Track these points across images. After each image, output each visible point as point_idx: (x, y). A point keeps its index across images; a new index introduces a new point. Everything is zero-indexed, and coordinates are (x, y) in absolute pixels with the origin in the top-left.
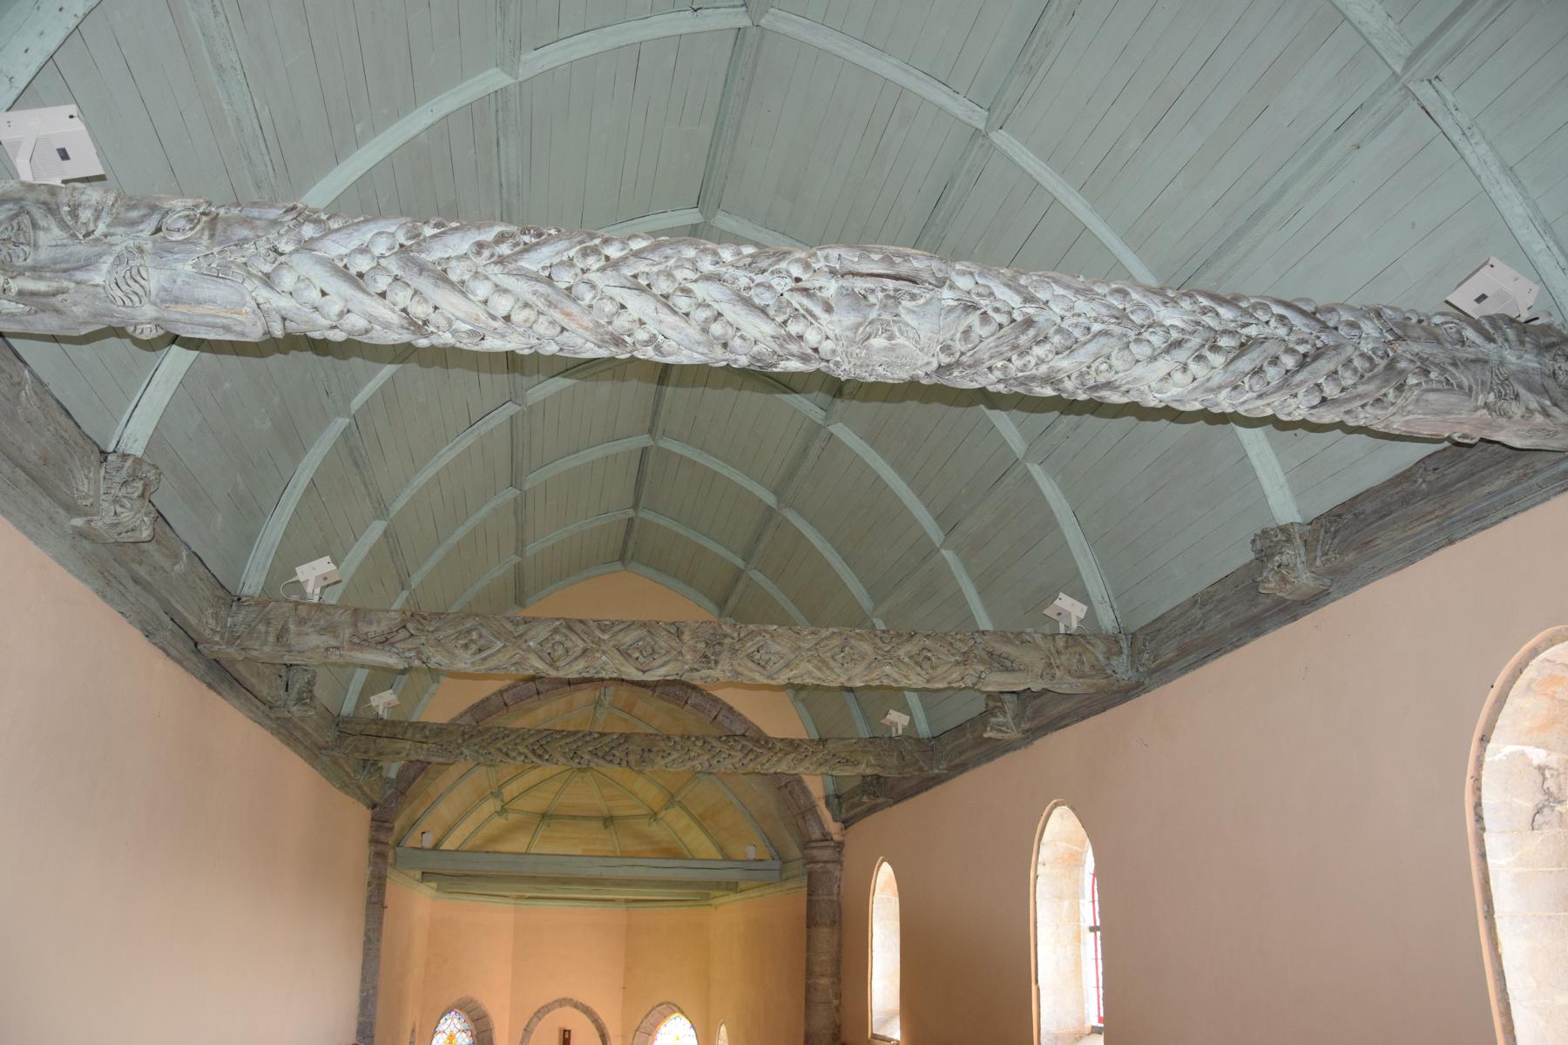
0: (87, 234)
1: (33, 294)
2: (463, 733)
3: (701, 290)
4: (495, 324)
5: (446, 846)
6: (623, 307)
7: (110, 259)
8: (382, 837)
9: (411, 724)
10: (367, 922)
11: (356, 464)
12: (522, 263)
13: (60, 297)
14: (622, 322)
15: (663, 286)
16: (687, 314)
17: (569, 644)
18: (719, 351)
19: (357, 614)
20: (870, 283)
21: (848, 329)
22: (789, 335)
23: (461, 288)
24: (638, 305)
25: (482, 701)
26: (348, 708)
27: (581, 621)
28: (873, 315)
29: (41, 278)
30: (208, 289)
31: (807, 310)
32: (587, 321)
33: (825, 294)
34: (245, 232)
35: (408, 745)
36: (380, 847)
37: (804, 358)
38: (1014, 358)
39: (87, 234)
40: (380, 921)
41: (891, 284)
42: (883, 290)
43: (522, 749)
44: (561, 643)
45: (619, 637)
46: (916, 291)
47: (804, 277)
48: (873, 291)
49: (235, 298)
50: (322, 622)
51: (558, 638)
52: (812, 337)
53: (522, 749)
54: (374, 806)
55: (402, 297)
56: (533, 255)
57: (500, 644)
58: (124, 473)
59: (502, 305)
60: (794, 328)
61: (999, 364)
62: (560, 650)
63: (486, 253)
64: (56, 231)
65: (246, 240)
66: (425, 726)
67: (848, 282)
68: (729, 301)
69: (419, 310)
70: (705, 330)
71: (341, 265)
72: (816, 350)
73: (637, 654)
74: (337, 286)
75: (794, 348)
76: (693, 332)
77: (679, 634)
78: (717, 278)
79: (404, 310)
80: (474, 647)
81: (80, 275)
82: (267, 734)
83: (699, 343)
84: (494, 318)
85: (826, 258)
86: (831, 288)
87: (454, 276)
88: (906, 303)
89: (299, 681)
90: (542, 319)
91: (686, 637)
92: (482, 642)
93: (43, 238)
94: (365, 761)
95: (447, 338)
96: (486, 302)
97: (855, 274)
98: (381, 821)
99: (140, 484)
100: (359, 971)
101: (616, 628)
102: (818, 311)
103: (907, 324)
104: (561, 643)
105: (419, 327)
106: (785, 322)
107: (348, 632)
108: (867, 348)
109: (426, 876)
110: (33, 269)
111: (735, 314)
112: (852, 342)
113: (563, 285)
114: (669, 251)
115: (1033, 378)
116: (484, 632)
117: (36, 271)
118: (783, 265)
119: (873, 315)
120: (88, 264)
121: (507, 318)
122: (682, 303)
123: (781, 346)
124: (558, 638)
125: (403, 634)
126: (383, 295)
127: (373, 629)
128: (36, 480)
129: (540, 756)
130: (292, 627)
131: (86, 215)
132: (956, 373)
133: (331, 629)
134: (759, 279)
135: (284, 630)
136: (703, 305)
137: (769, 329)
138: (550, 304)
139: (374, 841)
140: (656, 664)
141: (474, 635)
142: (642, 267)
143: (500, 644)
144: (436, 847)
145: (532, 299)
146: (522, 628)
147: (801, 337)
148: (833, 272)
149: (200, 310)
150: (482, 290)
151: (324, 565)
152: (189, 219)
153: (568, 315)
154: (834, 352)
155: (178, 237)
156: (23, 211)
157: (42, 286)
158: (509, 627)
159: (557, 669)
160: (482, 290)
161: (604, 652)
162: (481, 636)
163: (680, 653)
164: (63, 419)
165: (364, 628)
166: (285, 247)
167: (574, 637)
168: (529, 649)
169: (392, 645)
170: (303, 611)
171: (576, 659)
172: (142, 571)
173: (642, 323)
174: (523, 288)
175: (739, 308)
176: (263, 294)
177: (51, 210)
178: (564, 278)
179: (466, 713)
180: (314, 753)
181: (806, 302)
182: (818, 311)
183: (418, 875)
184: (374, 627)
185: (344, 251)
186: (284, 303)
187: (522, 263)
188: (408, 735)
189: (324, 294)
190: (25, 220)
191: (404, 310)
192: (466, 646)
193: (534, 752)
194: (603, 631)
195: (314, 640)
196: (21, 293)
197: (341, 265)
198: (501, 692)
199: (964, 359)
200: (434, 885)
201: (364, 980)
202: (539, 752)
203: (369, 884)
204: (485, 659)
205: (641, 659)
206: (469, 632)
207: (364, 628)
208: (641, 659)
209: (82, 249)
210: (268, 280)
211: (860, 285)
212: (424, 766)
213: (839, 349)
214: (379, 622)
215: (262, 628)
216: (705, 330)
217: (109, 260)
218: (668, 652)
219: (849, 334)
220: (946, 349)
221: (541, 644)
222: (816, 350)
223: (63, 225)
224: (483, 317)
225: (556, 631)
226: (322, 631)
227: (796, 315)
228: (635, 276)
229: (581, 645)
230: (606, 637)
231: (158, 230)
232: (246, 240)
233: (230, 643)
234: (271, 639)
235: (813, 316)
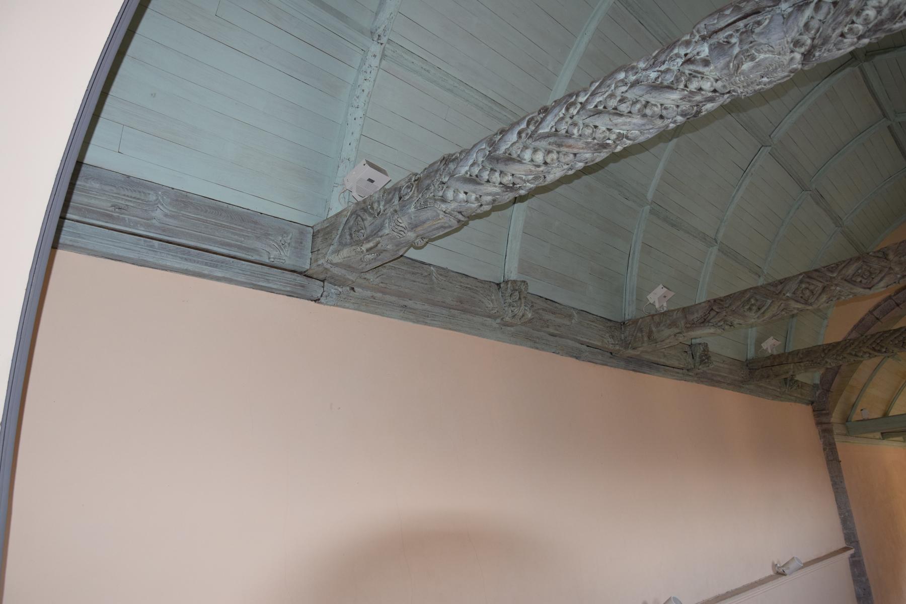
0: (378, 214)
1: (371, 249)
2: (824, 350)
3: (630, 95)
4: (541, 169)
5: (894, 412)
6: (596, 127)
7: (387, 221)
8: (824, 420)
9: (789, 353)
10: (830, 472)
11: (673, 226)
12: (541, 131)
13: (379, 245)
14: (599, 135)
15: (612, 103)
16: (630, 112)
17: (812, 287)
18: (659, 123)
19: (685, 311)
20: (729, 32)
21: (722, 69)
22: (691, 92)
23: (520, 161)
24: (602, 122)
25: (860, 321)
26: (751, 354)
27: (816, 270)
28: (736, 50)
29: (369, 241)
30: (426, 214)
31: (695, 71)
32: (581, 144)
33: (703, 55)
34: (428, 182)
35: (792, 366)
36: (825, 426)
37: (711, 100)
38: (854, 18)
39: (378, 214)
40: (840, 470)
41: (741, 24)
42: (737, 31)
43: (865, 349)
44: (807, 288)
45: (843, 272)
46: (759, 18)
47: (688, 51)
48: (731, 36)
49: (435, 214)
50: (668, 322)
51: (803, 286)
52: (707, 86)
53: (865, 349)
54: (812, 403)
55: (496, 177)
56: (545, 124)
57: (769, 301)
58: (509, 291)
59: (539, 157)
60: (693, 86)
61: (846, 30)
62: (807, 293)
63: (523, 135)
64: (369, 219)
65: (429, 185)
66: (798, 352)
67: (714, 40)
68: (647, 93)
69: (507, 179)
70: (644, 116)
71: (468, 176)
72: (715, 91)
73: (859, 279)
74: (469, 187)
75: (698, 98)
76: (637, 120)
77: (885, 256)
78: (636, 83)
79: (501, 183)
80: (754, 308)
81: (380, 234)
82: (695, 384)
83: (644, 125)
84: (539, 166)
85: (698, 31)
86: (705, 50)
87: (514, 156)
88: (757, 30)
89: (699, 351)
90: (561, 155)
91: (891, 257)
92: (759, 303)
93: (367, 223)
94: (786, 379)
95: (529, 186)
96: (532, 160)
97: (716, 32)
98: (821, 412)
99: (517, 293)
100: (835, 507)
101: (840, 267)
102: (700, 69)
103: (760, 44)
104: (807, 288)
105: (511, 188)
106: (686, 86)
107: (683, 322)
108: (743, 73)
109: (885, 435)
110: (367, 239)
111: (656, 98)
112: (730, 75)
113: (563, 132)
114: (609, 82)
115: (882, 23)
116: (758, 297)
117: (367, 239)
118: (676, 51)
119: (736, 50)
120: (382, 227)
121: (546, 163)
122: (624, 108)
123: (690, 101)
124: (803, 286)
125: (713, 314)
126: (488, 181)
127: (695, 316)
128: (464, 311)
129: (879, 351)
130: (654, 329)
131: (375, 206)
132: (817, 54)
133: (673, 324)
134: (663, 68)
135: (650, 333)
136: (634, 103)
137: (675, 96)
138: (560, 145)
139: (819, 424)
140: (875, 281)
141: (753, 301)
142: (598, 99)
143: (769, 301)
144: (885, 415)
145: (550, 147)
146: (780, 287)
147: (700, 89)
148: (704, 38)
149: (426, 226)
150: (527, 155)
151: (660, 291)
152: (408, 187)
153: (570, 146)
154: (724, 86)
155: (407, 197)
156: (358, 215)
157: (371, 244)
158: (772, 289)
159: (811, 304)
160: (527, 155)
161: (837, 285)
162: (757, 300)
163: (890, 268)
164: (464, 280)
165: (691, 318)
166: (445, 180)
167: (814, 282)
168: (788, 299)
169: (709, 322)
170: (657, 319)
171: (820, 294)
172: (551, 330)
173: (609, 130)
174: (543, 144)
175: (655, 94)
176: (444, 206)
177: (365, 210)
178: (563, 128)
179: (852, 331)
180: (737, 385)
181: (692, 67)
182: (700, 69)
183: (878, 435)
184: (696, 315)
185: (467, 168)
186: (453, 205)
187: (541, 131)
188: (790, 360)
189: (466, 193)
190: (359, 218)
191: (501, 183)
192: (750, 309)
193: (874, 349)
194: (832, 272)
195: (667, 332)
196: (367, 250)
197: (468, 176)
198: (871, 312)
199: (816, 41)
200: (901, 438)
201: (839, 508)
202: (878, 348)
203: (824, 449)
204: (763, 313)
205: (864, 281)
206: (749, 300)
207: (691, 318)
208: (864, 281)
209: (378, 222)
210: (443, 200)
211: (721, 37)
212: (836, 371)
213: (726, 84)
214: (697, 311)
215: (639, 335)
216: (644, 116)
217: (387, 221)
218: (881, 271)
219: (725, 71)
220: (797, 43)
221: (794, 293)
222: (715, 91)
223: (371, 214)
224: (533, 168)
225: (801, 282)
226: (670, 326)
227: (692, 76)
228: (596, 106)
229: (820, 285)
230: (835, 275)
231: (400, 198)
232: (429, 185)
233: (626, 347)
234: (646, 339)
235: (700, 73)
